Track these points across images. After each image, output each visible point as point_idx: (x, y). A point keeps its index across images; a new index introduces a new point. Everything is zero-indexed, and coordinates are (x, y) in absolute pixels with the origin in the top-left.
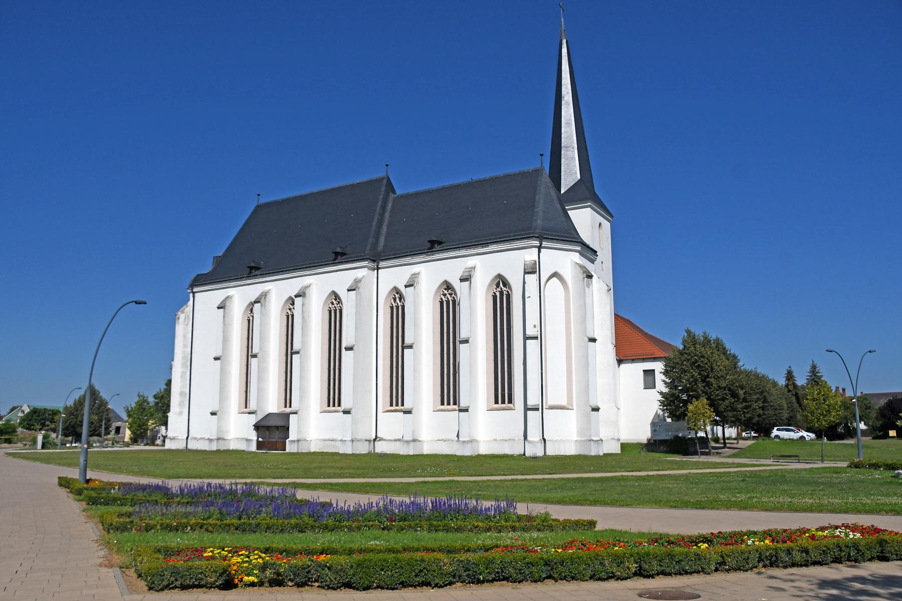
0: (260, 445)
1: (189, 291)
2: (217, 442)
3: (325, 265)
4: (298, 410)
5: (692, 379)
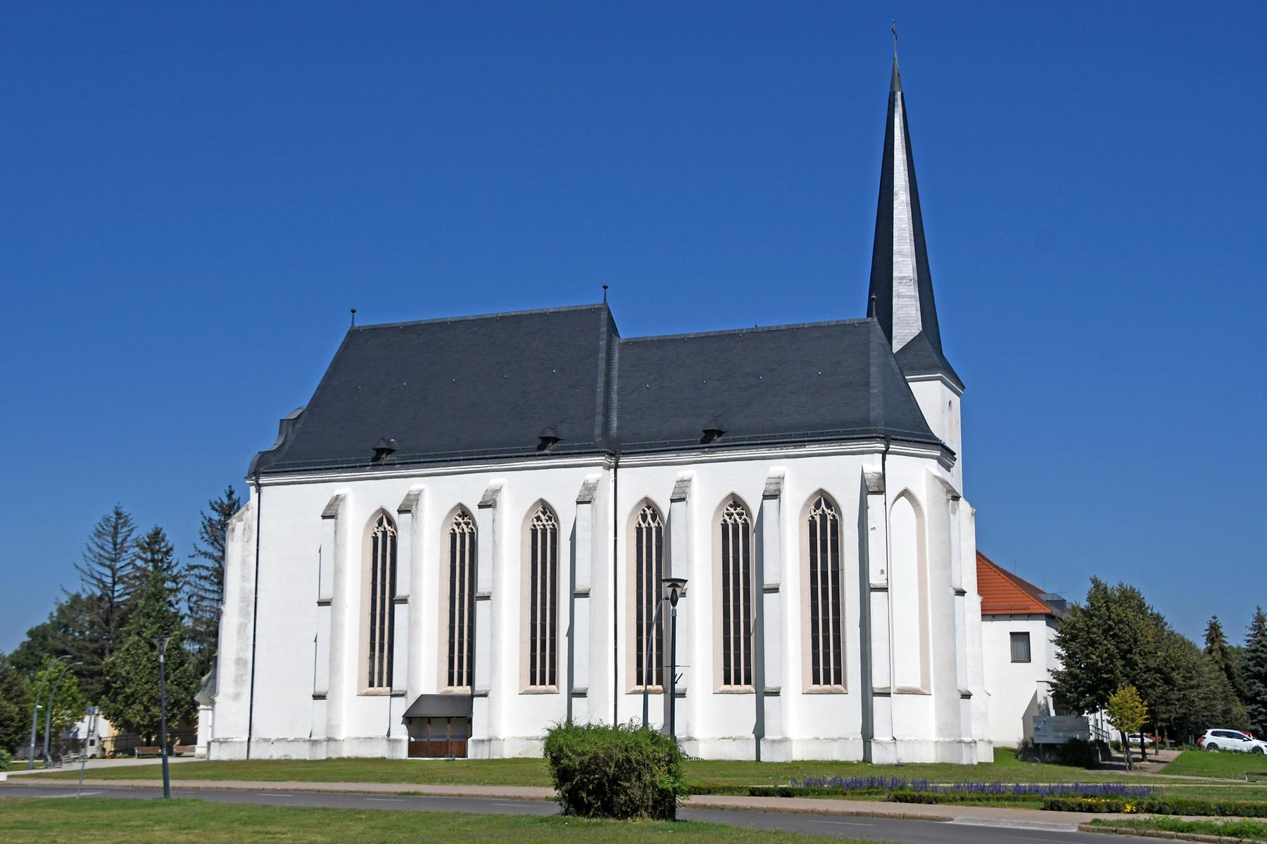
0: (414, 749)
1: (248, 482)
2: (328, 745)
3: (527, 456)
4: (489, 691)
5: (1105, 655)
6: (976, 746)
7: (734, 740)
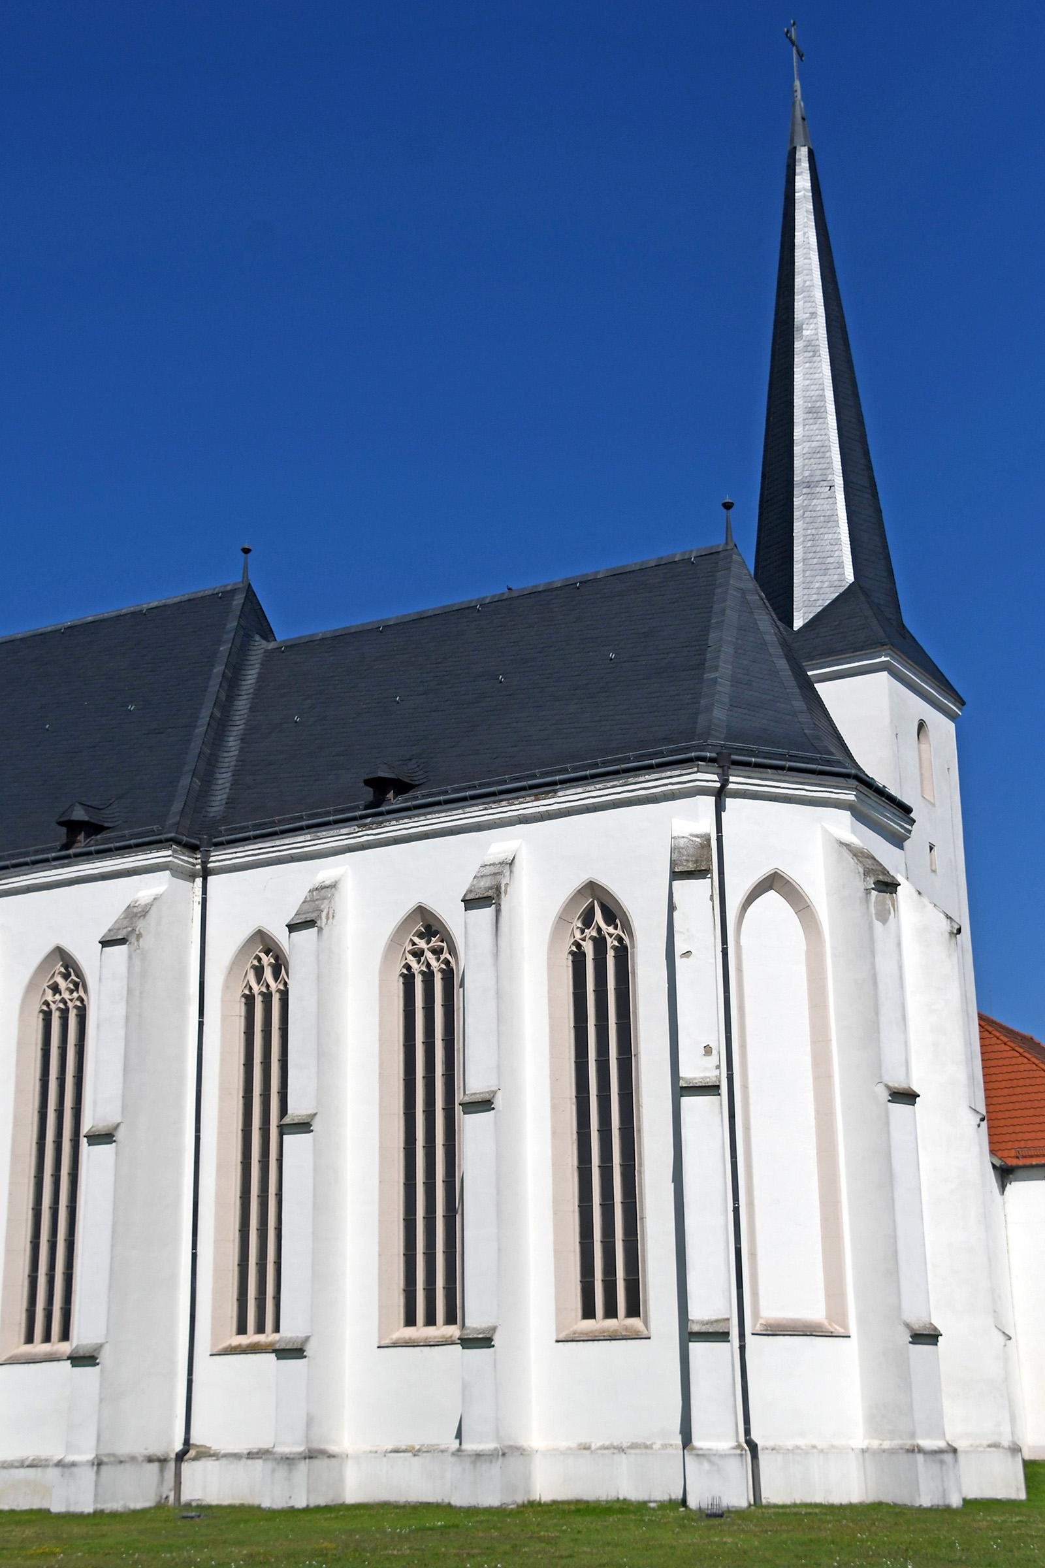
6: (956, 1460)
7: (416, 1452)
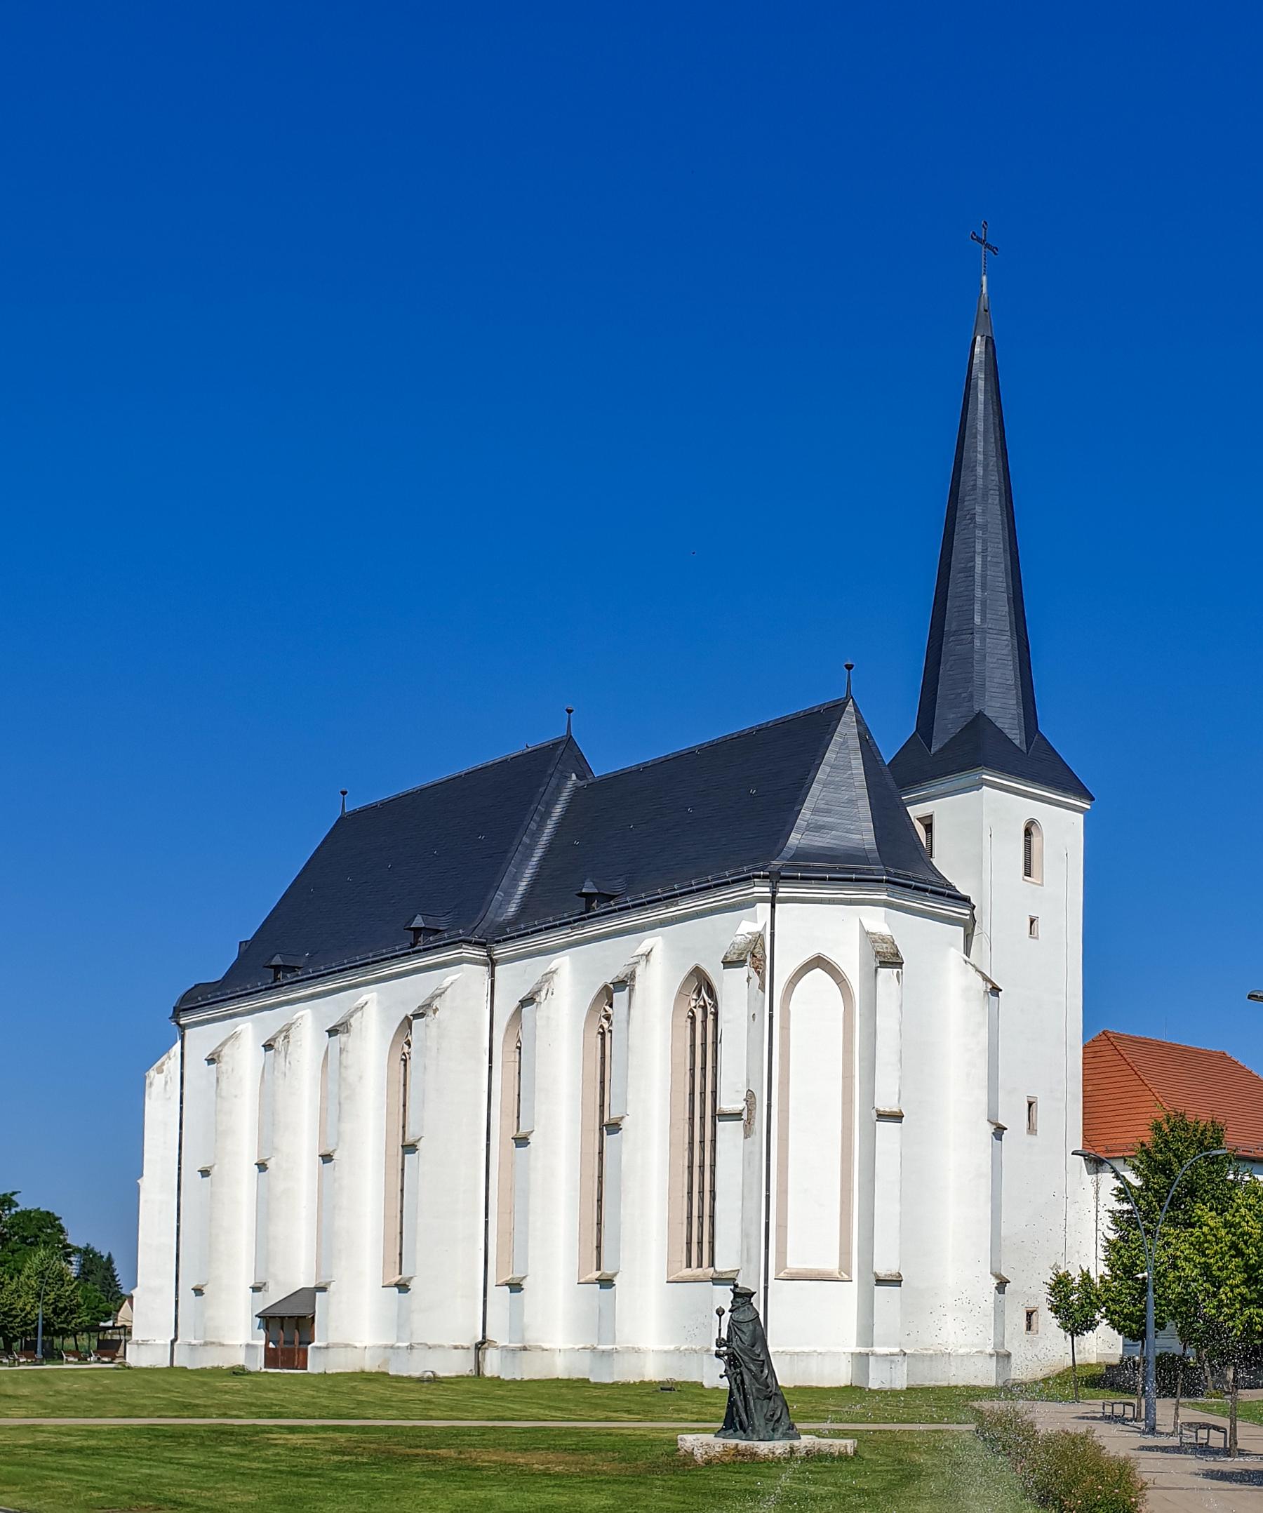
0: (272, 1359)
